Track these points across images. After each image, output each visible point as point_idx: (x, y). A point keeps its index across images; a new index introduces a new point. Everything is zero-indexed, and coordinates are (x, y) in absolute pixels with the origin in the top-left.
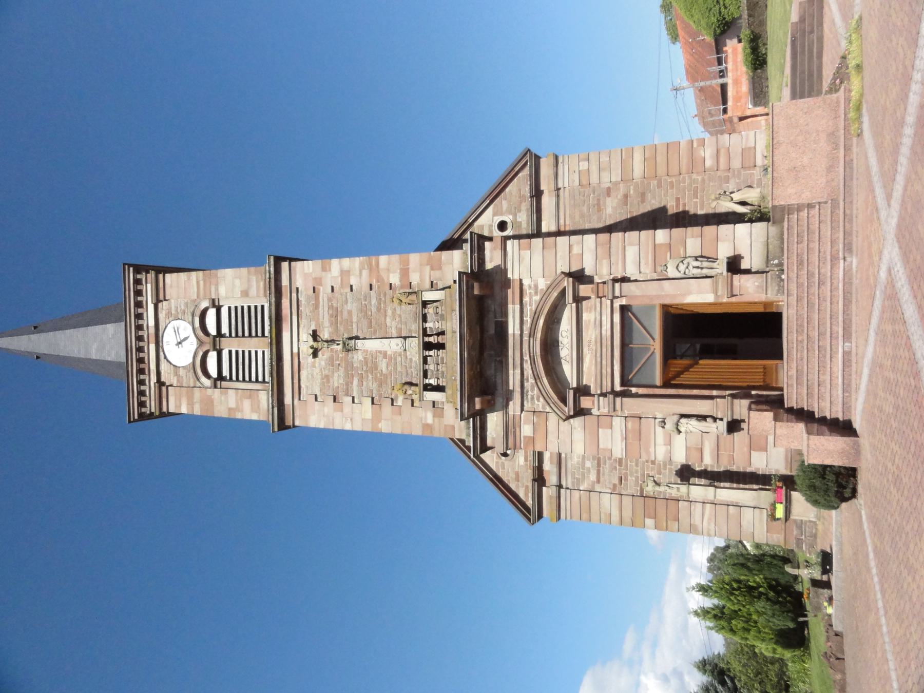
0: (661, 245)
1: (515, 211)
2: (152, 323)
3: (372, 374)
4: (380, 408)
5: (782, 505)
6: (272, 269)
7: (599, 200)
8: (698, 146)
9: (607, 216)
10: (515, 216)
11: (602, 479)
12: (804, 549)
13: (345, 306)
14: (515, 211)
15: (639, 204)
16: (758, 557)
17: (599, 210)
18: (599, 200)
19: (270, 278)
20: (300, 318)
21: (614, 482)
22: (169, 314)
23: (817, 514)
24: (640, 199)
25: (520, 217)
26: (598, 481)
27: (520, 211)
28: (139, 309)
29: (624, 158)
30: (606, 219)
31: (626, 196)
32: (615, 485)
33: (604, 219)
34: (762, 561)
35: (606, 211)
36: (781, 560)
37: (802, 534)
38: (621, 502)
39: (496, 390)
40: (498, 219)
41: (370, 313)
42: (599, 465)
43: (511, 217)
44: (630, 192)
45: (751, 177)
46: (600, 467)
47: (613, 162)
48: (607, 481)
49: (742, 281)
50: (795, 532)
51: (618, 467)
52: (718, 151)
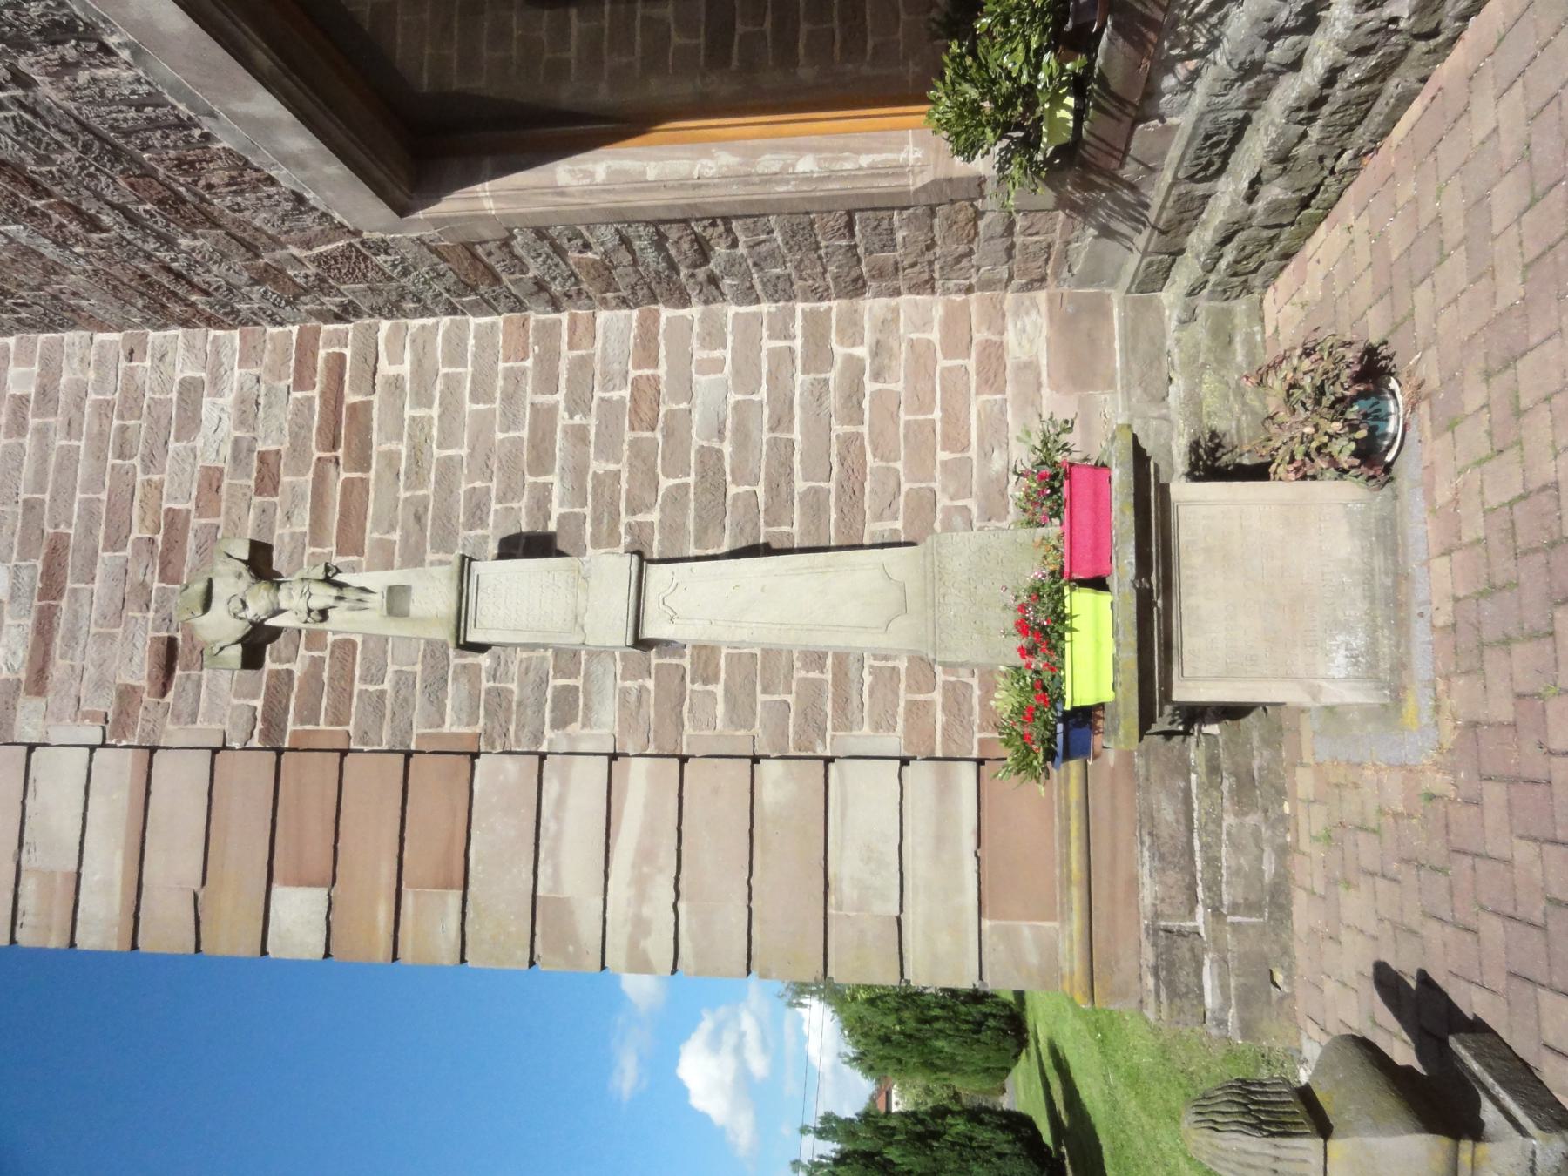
5: (1105, 599)
11: (58, 668)
12: (1210, 1000)
16: (922, 1122)
21: (125, 679)
23: (1372, 649)
26: (38, 679)
32: (127, 695)
34: (937, 1135)
36: (1003, 1128)
37: (1193, 900)
38: (148, 793)
42: (52, 585)
46: (60, 593)
48: (91, 673)
50: (1148, 893)
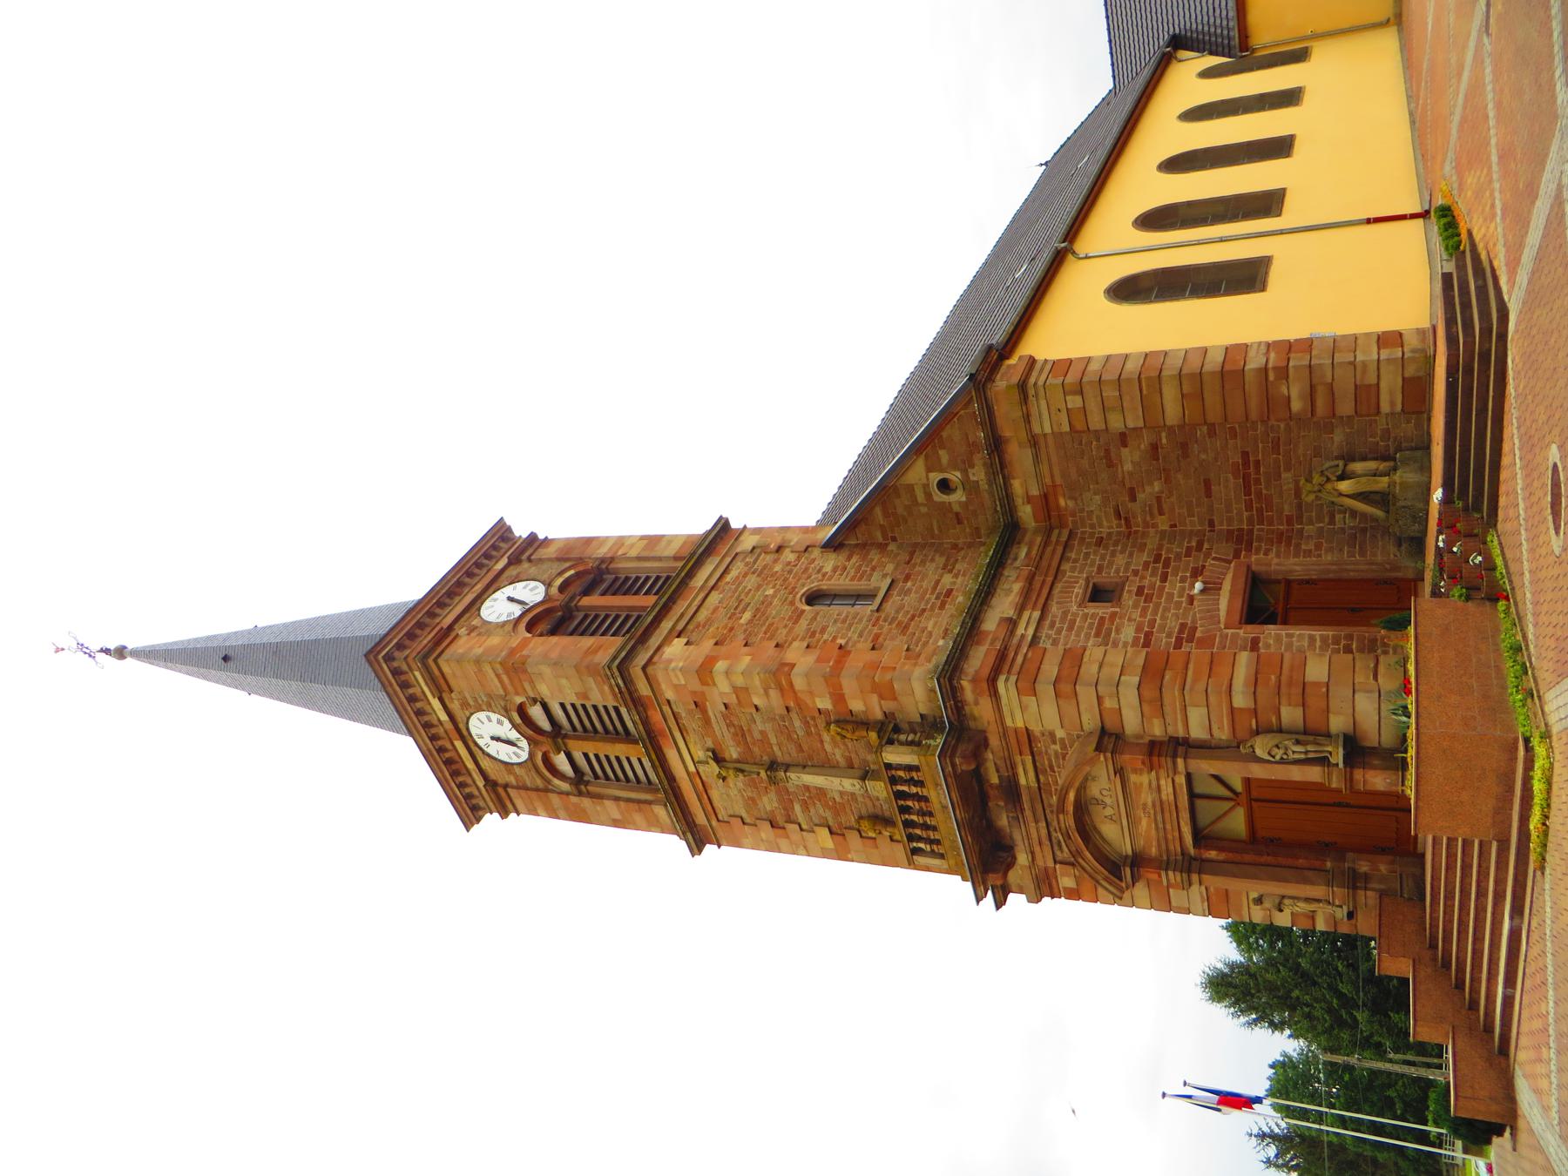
0: (1240, 709)
1: (966, 465)
2: (444, 717)
3: (820, 801)
4: (845, 839)
6: (620, 682)
7: (1107, 451)
8: (1278, 378)
9: (1127, 477)
10: (965, 472)
13: (753, 726)
14: (966, 465)
15: (1178, 458)
17: (1111, 465)
18: (1107, 451)
19: (621, 692)
20: (685, 735)
22: (465, 705)
24: (1180, 452)
25: (974, 474)
27: (972, 466)
28: (416, 704)
29: (1145, 392)
30: (1124, 478)
31: (1155, 447)
33: (1121, 479)
35: (1122, 467)
39: (1017, 845)
40: (936, 477)
41: (795, 736)
43: (958, 474)
44: (1161, 439)
45: (1371, 425)
47: (1126, 399)
49: (1367, 776)
51: (1158, 583)
52: (1312, 387)
